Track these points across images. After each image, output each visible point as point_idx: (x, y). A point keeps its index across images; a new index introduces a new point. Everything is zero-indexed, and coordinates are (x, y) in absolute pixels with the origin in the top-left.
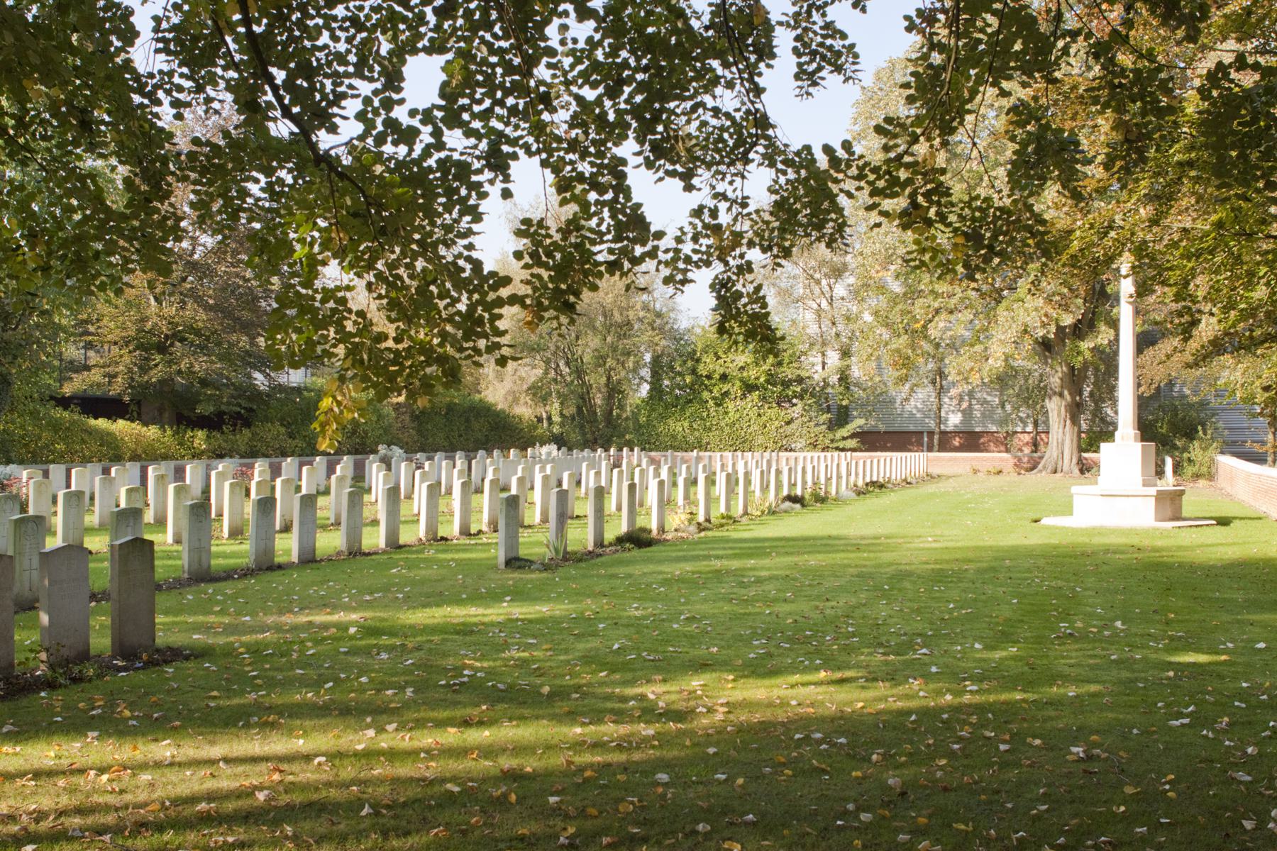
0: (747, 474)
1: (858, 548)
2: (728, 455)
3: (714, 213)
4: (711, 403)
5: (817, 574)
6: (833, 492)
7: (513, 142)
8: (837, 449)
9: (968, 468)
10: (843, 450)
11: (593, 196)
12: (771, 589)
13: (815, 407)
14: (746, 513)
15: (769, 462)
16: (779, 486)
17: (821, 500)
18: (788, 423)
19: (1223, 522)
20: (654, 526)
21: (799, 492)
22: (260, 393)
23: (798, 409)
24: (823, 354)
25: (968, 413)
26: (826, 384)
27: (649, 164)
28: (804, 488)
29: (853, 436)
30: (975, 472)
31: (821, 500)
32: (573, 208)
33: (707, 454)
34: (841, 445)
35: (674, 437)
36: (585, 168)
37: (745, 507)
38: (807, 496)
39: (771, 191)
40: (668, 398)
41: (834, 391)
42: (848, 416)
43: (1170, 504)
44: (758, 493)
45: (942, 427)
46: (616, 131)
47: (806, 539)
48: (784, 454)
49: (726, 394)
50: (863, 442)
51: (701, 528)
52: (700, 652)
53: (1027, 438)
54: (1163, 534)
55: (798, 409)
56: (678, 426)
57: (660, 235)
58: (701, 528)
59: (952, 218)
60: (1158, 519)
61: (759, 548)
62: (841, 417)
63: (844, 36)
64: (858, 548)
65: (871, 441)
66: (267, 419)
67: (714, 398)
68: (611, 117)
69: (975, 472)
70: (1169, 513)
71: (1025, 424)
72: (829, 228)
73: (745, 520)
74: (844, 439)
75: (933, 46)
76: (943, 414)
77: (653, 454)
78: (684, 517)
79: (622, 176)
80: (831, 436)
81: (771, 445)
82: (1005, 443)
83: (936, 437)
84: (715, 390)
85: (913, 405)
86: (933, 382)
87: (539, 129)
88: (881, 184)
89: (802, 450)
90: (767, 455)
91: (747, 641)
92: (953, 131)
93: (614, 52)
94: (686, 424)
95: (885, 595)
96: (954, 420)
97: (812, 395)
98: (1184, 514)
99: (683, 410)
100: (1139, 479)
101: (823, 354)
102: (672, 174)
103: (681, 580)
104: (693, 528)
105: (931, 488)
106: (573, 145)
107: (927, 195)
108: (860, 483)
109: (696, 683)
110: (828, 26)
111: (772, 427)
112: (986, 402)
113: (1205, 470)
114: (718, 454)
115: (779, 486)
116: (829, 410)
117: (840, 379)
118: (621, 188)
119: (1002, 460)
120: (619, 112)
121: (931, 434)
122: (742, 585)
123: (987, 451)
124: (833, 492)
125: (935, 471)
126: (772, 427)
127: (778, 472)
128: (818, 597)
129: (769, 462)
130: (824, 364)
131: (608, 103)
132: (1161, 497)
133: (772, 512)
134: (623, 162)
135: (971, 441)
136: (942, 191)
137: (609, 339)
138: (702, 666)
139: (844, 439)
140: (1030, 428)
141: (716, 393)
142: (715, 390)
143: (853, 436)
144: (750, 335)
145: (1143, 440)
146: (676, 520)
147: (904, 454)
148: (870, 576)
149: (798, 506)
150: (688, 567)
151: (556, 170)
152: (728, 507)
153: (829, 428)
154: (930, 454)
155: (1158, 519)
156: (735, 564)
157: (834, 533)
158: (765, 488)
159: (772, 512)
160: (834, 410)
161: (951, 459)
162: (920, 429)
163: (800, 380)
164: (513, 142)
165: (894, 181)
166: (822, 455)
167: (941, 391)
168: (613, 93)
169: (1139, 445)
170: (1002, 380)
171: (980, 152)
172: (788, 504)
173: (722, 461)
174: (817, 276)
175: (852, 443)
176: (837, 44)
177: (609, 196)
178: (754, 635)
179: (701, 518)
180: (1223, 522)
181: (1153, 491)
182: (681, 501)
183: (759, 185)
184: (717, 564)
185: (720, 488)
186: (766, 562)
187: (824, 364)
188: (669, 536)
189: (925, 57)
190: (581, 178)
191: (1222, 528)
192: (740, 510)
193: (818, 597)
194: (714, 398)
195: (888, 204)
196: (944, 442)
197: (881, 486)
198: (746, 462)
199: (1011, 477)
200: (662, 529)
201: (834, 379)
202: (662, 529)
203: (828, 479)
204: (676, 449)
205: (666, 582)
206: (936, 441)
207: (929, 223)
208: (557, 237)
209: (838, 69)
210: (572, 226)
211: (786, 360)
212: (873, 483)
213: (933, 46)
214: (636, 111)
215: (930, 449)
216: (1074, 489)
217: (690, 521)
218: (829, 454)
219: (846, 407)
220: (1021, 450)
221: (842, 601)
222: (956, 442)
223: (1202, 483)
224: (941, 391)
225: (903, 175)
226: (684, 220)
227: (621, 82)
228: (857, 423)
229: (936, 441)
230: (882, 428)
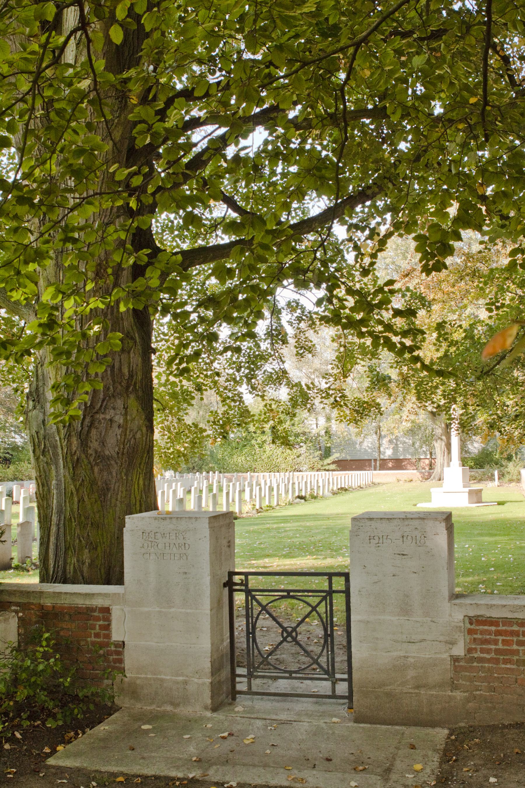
0: (278, 486)
2: (267, 474)
3: (270, 405)
4: (257, 446)
5: (309, 528)
6: (321, 493)
7: (206, 385)
8: (325, 470)
9: (395, 479)
10: (328, 470)
11: (233, 404)
12: (291, 534)
13: (312, 448)
14: (278, 505)
15: (288, 479)
17: (314, 497)
18: (298, 457)
19: (500, 503)
20: (237, 510)
21: (303, 494)
23: (303, 449)
24: (317, 419)
25: (395, 449)
26: (319, 435)
27: (250, 392)
28: (306, 492)
30: (398, 481)
31: (314, 497)
32: (226, 407)
33: (256, 474)
34: (327, 468)
36: (230, 395)
37: (278, 501)
38: (308, 496)
39: (288, 394)
40: (234, 444)
41: (323, 439)
42: (330, 451)
43: (476, 496)
44: (283, 495)
45: (382, 457)
47: (306, 515)
48: (296, 474)
49: (264, 442)
50: (338, 466)
51: (258, 512)
52: (267, 552)
53: (427, 462)
55: (303, 449)
56: (240, 459)
57: (254, 415)
58: (258, 512)
59: (349, 405)
60: (470, 503)
61: (285, 519)
62: (327, 453)
63: (311, 342)
65: (343, 465)
66: (20, 460)
67: (258, 444)
69: (398, 481)
70: (475, 500)
71: (426, 454)
73: (278, 508)
74: (329, 464)
75: (341, 346)
76: (382, 449)
78: (250, 507)
79: (241, 398)
80: (321, 463)
81: (289, 468)
82: (415, 464)
83: (378, 462)
84: (259, 439)
87: (215, 383)
88: (324, 395)
89: (306, 471)
90: (287, 474)
91: (283, 549)
92: (347, 377)
93: (238, 358)
94: (243, 458)
96: (388, 453)
97: (311, 441)
98: (483, 500)
99: (241, 450)
100: (461, 484)
101: (317, 419)
102: (258, 395)
103: (253, 532)
104: (255, 512)
105: (372, 490)
106: (226, 388)
107: (340, 397)
108: (335, 488)
109: (267, 560)
110: (306, 338)
111: (290, 459)
112: (405, 442)
113: (515, 477)
114: (262, 474)
116: (320, 449)
117: (326, 432)
118: (241, 401)
119: (412, 474)
120: (241, 377)
121: (375, 460)
122: (278, 532)
123: (406, 469)
124: (321, 493)
125: (376, 481)
126: (290, 459)
127: (293, 484)
129: (288, 479)
131: (237, 374)
132: (471, 492)
133: (290, 504)
134: (242, 393)
135: (398, 464)
136: (343, 396)
137: (201, 413)
138: (268, 556)
139: (329, 464)
140: (428, 457)
141: (259, 441)
143: (333, 463)
144: (282, 443)
146: (247, 508)
147: (362, 472)
148: (331, 529)
149: (303, 501)
151: (221, 396)
152: (270, 502)
158: (287, 492)
159: (290, 504)
161: (385, 474)
162: (370, 458)
163: (304, 434)
164: (206, 385)
165: (328, 394)
166: (316, 473)
167: (380, 437)
168: (238, 371)
169: (461, 468)
170: (412, 432)
171: (356, 385)
172: (298, 500)
173: (266, 478)
174: (313, 377)
175: (333, 467)
176: (310, 344)
177: (238, 403)
178: (285, 547)
179: (257, 507)
180: (500, 503)
181: (467, 490)
182: (248, 500)
183: (283, 393)
184: (268, 526)
185: (266, 491)
186: (289, 525)
188: (244, 515)
189: (339, 349)
190: (229, 398)
191: (500, 506)
194: (258, 444)
195: (326, 401)
196: (383, 465)
197: (346, 490)
198: (275, 479)
200: (240, 512)
201: (323, 433)
202: (240, 512)
203: (318, 487)
204: (237, 471)
205: (247, 532)
206: (378, 464)
207: (341, 406)
208: (221, 416)
209: (310, 352)
210: (225, 413)
211: (296, 423)
212: (342, 488)
213: (341, 346)
214: (246, 376)
215: (375, 469)
216: (432, 490)
218: (320, 473)
219: (329, 447)
220: (424, 468)
221: (319, 538)
222: (390, 465)
223: (513, 484)
224: (380, 437)
225: (331, 392)
227: (241, 367)
228: (336, 456)
229: (378, 464)
230: (349, 458)
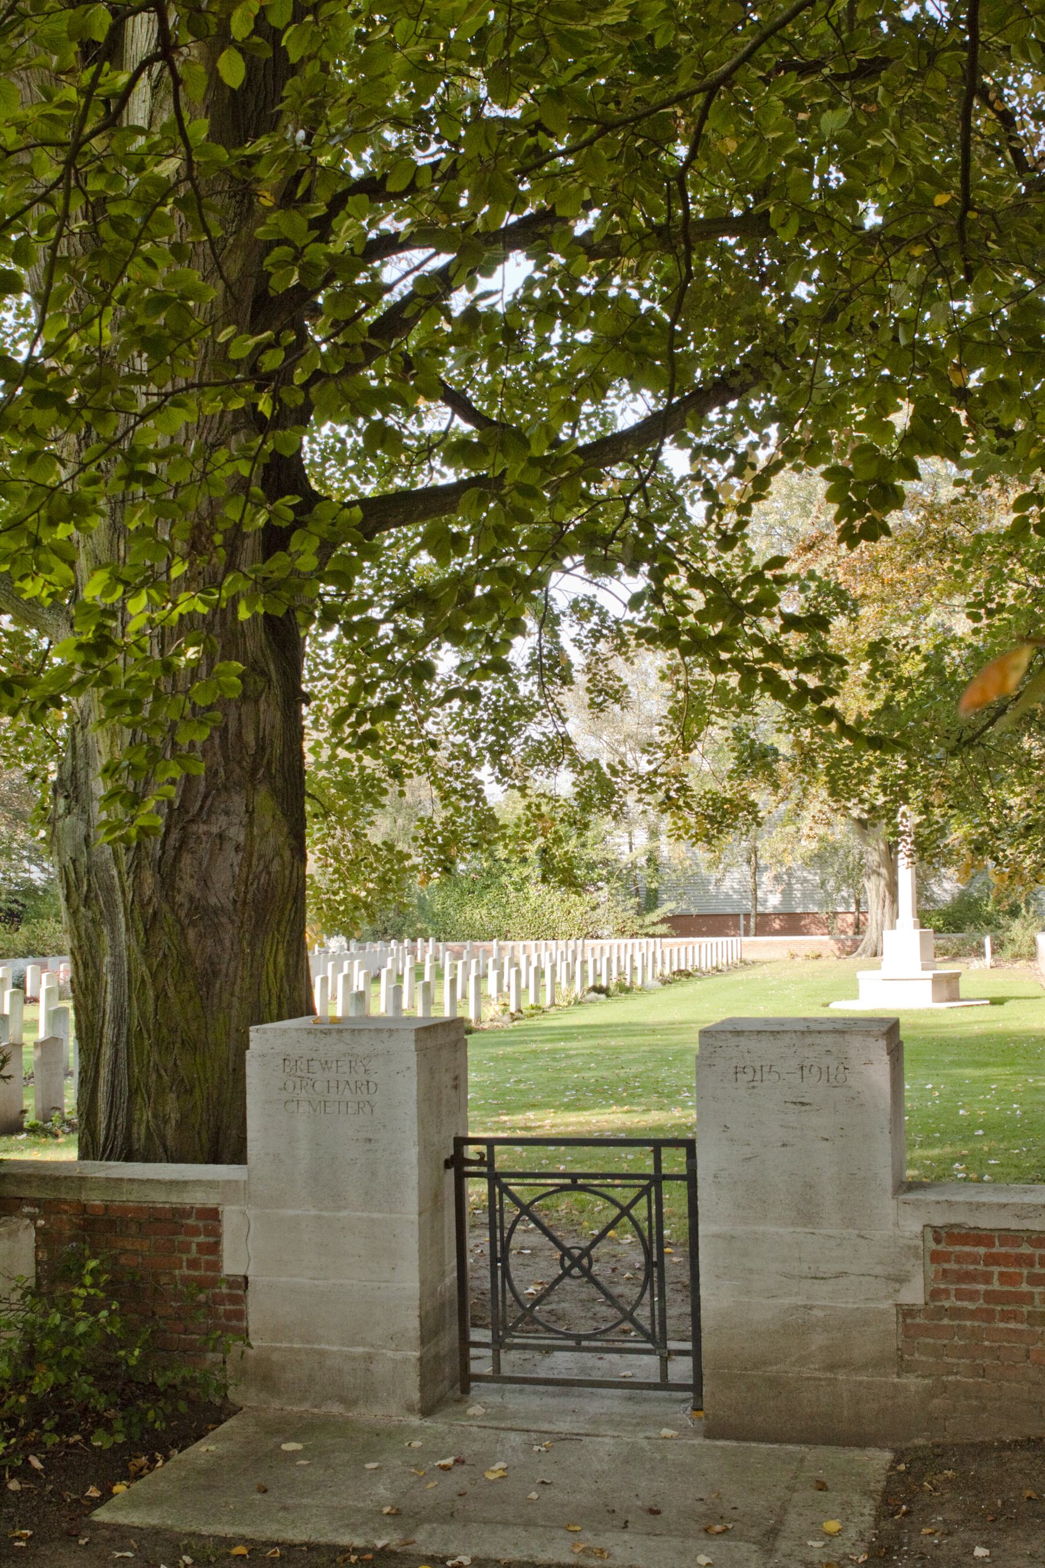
1: (654, 1032)
2: (531, 944)
4: (511, 888)
5: (616, 1052)
6: (639, 982)
7: (410, 767)
8: (647, 935)
10: (653, 936)
11: (463, 804)
12: (579, 1062)
14: (553, 1004)
15: (574, 952)
16: (584, 977)
18: (594, 909)
19: (996, 1002)
20: (471, 1015)
21: (604, 984)
22: (36, 889)
23: (604, 894)
24: (630, 834)
25: (787, 894)
26: (634, 866)
27: (498, 781)
28: (609, 979)
29: (663, 921)
30: (793, 956)
32: (451, 811)
33: (510, 943)
34: (651, 931)
35: (471, 926)
36: (458, 786)
37: (553, 998)
38: (612, 987)
40: (465, 885)
41: (643, 874)
42: (656, 898)
43: (947, 987)
45: (760, 909)
46: (473, 762)
48: (590, 943)
49: (526, 879)
50: (673, 927)
51: (514, 1018)
52: (531, 1099)
53: (850, 918)
54: (932, 1013)
55: (604, 894)
56: (477, 914)
57: (505, 827)
58: (514, 1018)
59: (694, 805)
60: (935, 1001)
61: (568, 1033)
62: (651, 901)
63: (620, 680)
64: (654, 1032)
65: (683, 925)
66: (40, 916)
67: (513, 883)
68: (474, 753)
69: (793, 956)
70: (946, 995)
71: (848, 904)
72: (614, 808)
73: (553, 1010)
74: (654, 924)
75: (678, 688)
76: (760, 894)
77: (450, 944)
78: (499, 1008)
79: (481, 791)
80: (639, 922)
81: (575, 932)
82: (827, 923)
83: (752, 920)
84: (515, 873)
85: (727, 884)
86: (749, 862)
89: (609, 937)
90: (571, 943)
91: (563, 1093)
92: (690, 750)
93: (474, 712)
94: (484, 912)
95: (668, 1063)
96: (773, 901)
97: (619, 879)
99: (480, 895)
100: (919, 964)
101: (630, 834)
102: (513, 786)
104: (507, 1018)
105: (739, 976)
106: (449, 772)
107: (677, 790)
108: (667, 972)
109: (530, 1115)
110: (609, 672)
111: (577, 913)
113: (1025, 950)
114: (522, 943)
115: (584, 977)
116: (637, 893)
117: (649, 860)
118: (480, 798)
119: (821, 943)
120: (480, 750)
121: (747, 916)
122: (554, 1059)
123: (808, 934)
124: (639, 982)
125: (748, 956)
126: (577, 913)
127: (584, 962)
128: (616, 1067)
129: (574, 952)
130: (631, 844)
131: (472, 744)
132: (937, 980)
133: (578, 1003)
134: (482, 782)
135: (793, 923)
136: (683, 789)
137: (400, 821)
138: (533, 1106)
139: (654, 924)
140: (853, 909)
141: (515, 878)
142: (515, 873)
143: (663, 921)
144: (562, 882)
145: (922, 927)
146: (491, 1011)
147: (720, 940)
148: (660, 1052)
149: (603, 996)
150: (509, 1049)
151: (440, 788)
152: (537, 999)
153: (638, 914)
154: (745, 939)
155: (935, 1001)
156: (547, 1046)
157: (634, 1020)
158: (571, 979)
159: (578, 1003)
160: (643, 893)
161: (767, 944)
162: (737, 911)
163: (605, 863)
164: (410, 767)
165: (653, 784)
166: (630, 941)
167: (757, 870)
168: (474, 737)
169: (917, 932)
170: (819, 859)
171: (708, 765)
172: (593, 994)
173: (529, 952)
174: (622, 749)
175: (663, 929)
176: (616, 685)
178: (567, 1088)
179: (513, 1009)
180: (996, 1002)
181: (929, 974)
183: (563, 783)
185: (529, 977)
186: (574, 1044)
187: (631, 844)
188: (486, 1026)
189: (674, 695)
191: (996, 1008)
192: (548, 1002)
193: (616, 1067)
194: (513, 883)
195: (648, 798)
196: (763, 925)
197: (689, 975)
199: (830, 962)
200: (478, 1018)
201: (642, 861)
202: (478, 1018)
203: (634, 969)
204: (472, 938)
207: (679, 808)
208: (440, 828)
209: (617, 701)
210: (448, 821)
211: (590, 842)
212: (680, 972)
213: (678, 688)
214: (490, 748)
215: (747, 934)
216: (860, 975)
217: (504, 1012)
218: (636, 941)
219: (656, 890)
220: (843, 932)
222: (777, 925)
223: (1022, 963)
224: (757, 870)
225: (659, 780)
226: (520, 810)
228: (668, 907)
230: (694, 911)
